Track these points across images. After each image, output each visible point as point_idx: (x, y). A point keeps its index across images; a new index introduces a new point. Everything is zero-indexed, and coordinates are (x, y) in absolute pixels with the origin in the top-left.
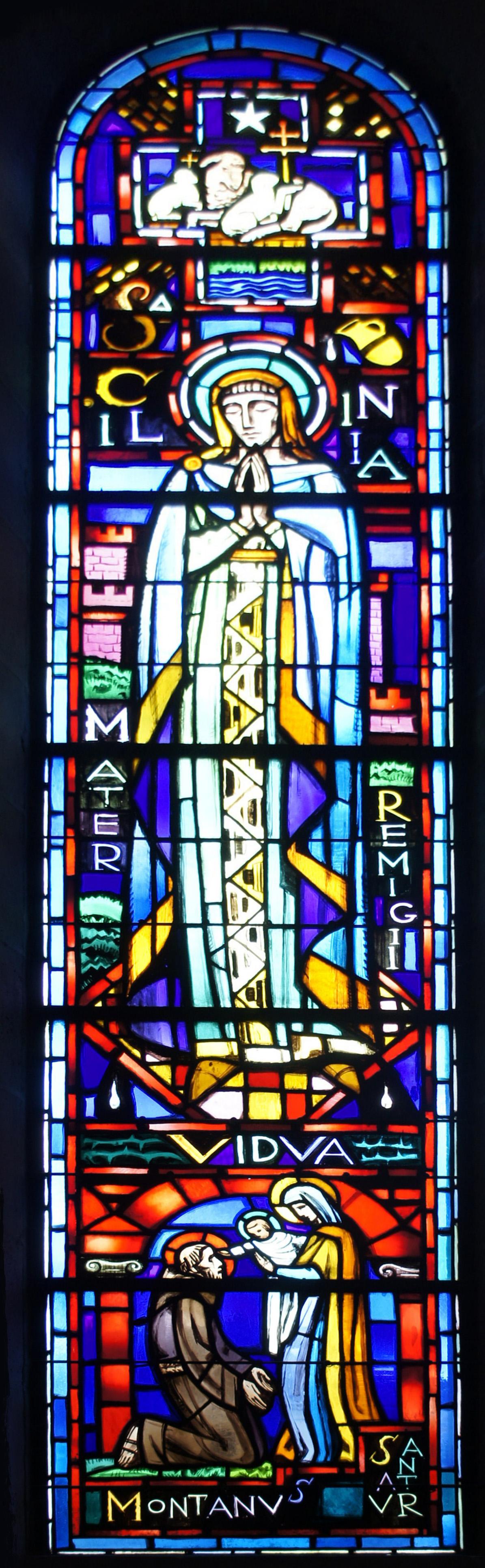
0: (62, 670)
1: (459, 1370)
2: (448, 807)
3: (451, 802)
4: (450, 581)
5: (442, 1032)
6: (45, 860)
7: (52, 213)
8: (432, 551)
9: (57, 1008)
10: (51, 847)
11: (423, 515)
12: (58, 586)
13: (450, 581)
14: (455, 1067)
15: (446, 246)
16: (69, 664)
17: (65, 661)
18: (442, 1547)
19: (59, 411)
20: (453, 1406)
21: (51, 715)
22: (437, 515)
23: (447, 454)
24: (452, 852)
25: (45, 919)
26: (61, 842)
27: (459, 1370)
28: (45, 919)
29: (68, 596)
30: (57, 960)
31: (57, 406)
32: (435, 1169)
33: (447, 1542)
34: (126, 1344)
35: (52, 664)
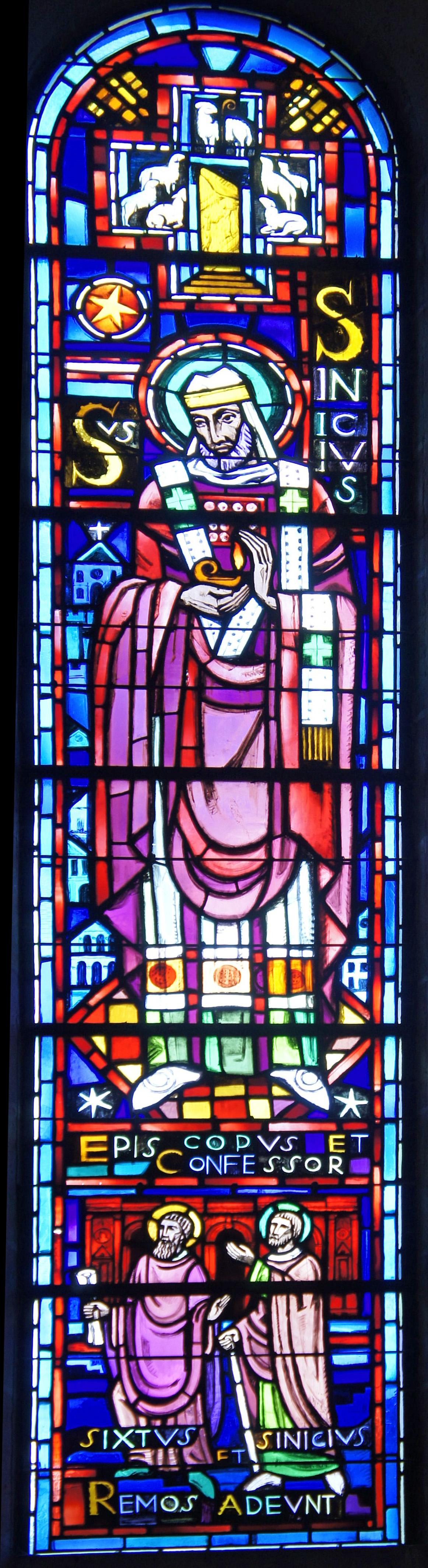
0: (47, 951)
1: (397, 176)
2: (395, 308)
3: (400, 991)
4: (401, 942)
5: (390, 1043)
6: (35, 583)
7: (34, 909)
8: (385, 979)
9: (44, 508)
10: (39, 366)
11: (374, 279)
12: (39, 357)
13: (401, 942)
14: (400, 999)
15: (400, 1278)
16: (54, 945)
17: (51, 941)
18: (385, 1539)
19: (43, 734)
20: (398, 1506)
21: (38, 1326)
22: (387, 279)
23: (401, 1355)
24: (398, 423)
25: (35, 1182)
26: (46, 141)
27: (397, 176)
28: (35, 1182)
29: (53, 959)
30: (41, 184)
31: (41, 730)
32: (380, 574)
33: (389, 1536)
34: (105, 191)
35: (37, 354)
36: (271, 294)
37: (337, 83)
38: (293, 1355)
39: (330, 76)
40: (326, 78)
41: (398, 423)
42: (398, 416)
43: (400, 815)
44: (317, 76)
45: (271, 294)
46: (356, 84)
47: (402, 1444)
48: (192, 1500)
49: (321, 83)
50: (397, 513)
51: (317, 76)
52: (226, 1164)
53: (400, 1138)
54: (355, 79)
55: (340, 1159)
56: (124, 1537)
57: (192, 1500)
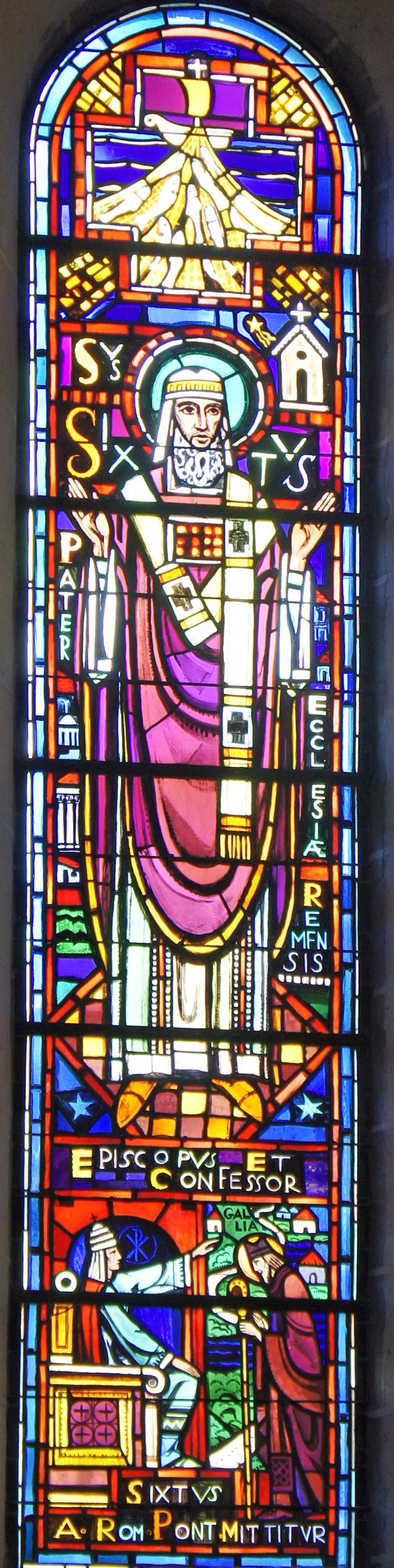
4: (357, 862)
13: (357, 862)
24: (357, 739)
36: (313, 754)
37: (298, 68)
38: (224, 599)
39: (292, 62)
40: (287, 63)
41: (357, 739)
42: (358, 634)
43: (357, 876)
44: (278, 60)
45: (313, 754)
46: (314, 70)
47: (358, 678)
48: (115, 374)
49: (282, 67)
50: (355, 1298)
51: (278, 60)
52: (309, 940)
53: (359, 182)
54: (312, 65)
55: (318, 888)
56: (48, 200)
57: (115, 374)
